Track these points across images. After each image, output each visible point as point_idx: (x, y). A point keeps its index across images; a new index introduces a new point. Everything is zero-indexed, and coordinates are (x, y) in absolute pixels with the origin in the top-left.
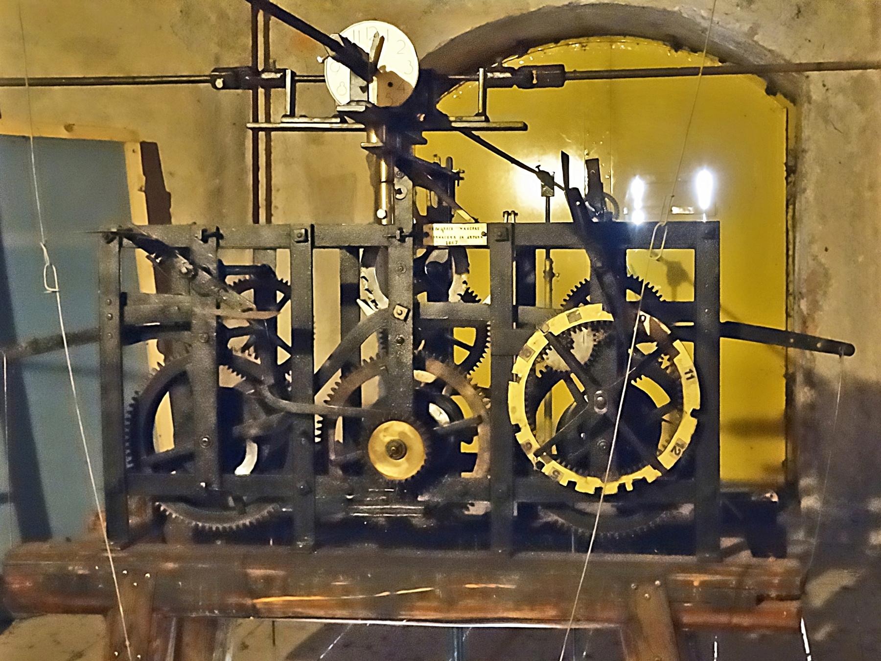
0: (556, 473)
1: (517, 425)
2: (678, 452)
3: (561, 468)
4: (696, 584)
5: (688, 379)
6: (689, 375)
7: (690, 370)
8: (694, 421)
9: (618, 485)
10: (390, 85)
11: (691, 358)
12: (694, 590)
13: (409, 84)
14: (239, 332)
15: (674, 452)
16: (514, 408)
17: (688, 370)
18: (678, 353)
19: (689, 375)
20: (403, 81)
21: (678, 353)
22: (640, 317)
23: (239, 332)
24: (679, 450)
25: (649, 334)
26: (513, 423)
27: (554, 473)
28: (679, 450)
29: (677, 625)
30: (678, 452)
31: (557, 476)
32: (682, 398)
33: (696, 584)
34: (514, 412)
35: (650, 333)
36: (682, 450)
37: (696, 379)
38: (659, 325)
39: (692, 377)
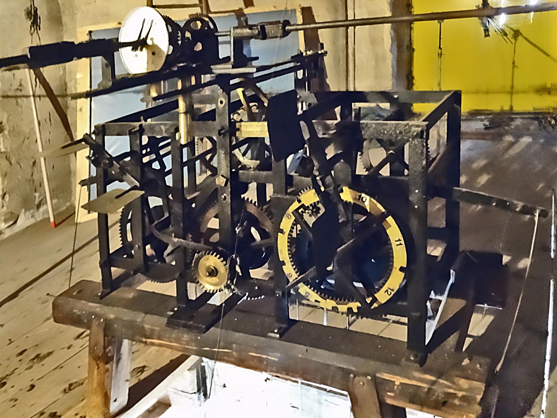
0: (307, 294)
1: (283, 261)
2: (389, 293)
3: (310, 291)
4: (397, 383)
5: (397, 245)
6: (398, 243)
7: (399, 239)
8: (402, 275)
9: (347, 308)
10: (153, 54)
11: (79, 279)
12: (396, 387)
13: (163, 52)
14: (381, 165)
15: (386, 293)
16: (281, 250)
17: (398, 240)
18: (390, 226)
19: (398, 243)
20: (161, 50)
21: (390, 226)
22: (363, 198)
23: (381, 165)
24: (391, 293)
25: (369, 211)
26: (281, 260)
27: (306, 293)
28: (391, 293)
29: (382, 404)
30: (389, 293)
31: (308, 296)
32: (393, 257)
33: (397, 383)
34: (281, 253)
35: (370, 210)
36: (393, 293)
37: (404, 245)
38: (376, 205)
39: (401, 244)
